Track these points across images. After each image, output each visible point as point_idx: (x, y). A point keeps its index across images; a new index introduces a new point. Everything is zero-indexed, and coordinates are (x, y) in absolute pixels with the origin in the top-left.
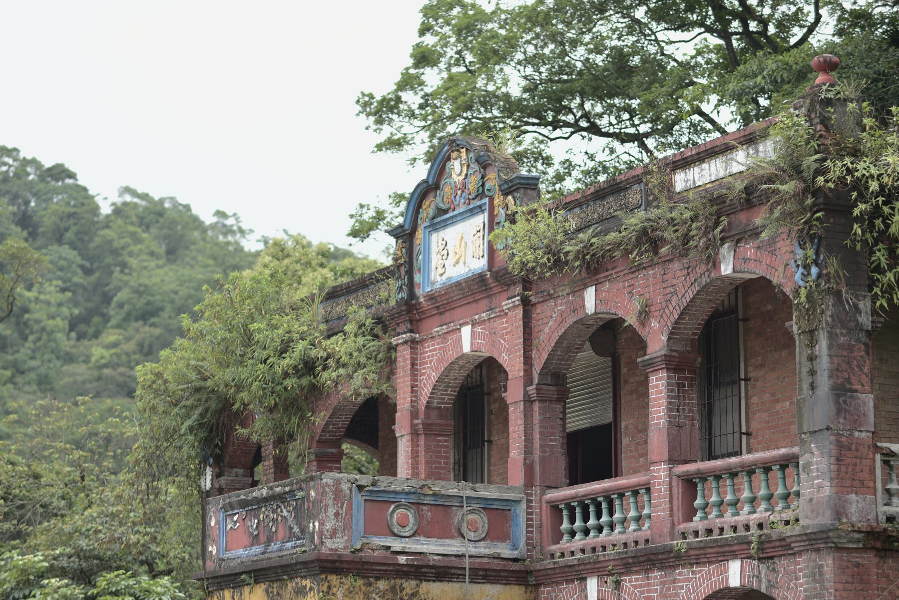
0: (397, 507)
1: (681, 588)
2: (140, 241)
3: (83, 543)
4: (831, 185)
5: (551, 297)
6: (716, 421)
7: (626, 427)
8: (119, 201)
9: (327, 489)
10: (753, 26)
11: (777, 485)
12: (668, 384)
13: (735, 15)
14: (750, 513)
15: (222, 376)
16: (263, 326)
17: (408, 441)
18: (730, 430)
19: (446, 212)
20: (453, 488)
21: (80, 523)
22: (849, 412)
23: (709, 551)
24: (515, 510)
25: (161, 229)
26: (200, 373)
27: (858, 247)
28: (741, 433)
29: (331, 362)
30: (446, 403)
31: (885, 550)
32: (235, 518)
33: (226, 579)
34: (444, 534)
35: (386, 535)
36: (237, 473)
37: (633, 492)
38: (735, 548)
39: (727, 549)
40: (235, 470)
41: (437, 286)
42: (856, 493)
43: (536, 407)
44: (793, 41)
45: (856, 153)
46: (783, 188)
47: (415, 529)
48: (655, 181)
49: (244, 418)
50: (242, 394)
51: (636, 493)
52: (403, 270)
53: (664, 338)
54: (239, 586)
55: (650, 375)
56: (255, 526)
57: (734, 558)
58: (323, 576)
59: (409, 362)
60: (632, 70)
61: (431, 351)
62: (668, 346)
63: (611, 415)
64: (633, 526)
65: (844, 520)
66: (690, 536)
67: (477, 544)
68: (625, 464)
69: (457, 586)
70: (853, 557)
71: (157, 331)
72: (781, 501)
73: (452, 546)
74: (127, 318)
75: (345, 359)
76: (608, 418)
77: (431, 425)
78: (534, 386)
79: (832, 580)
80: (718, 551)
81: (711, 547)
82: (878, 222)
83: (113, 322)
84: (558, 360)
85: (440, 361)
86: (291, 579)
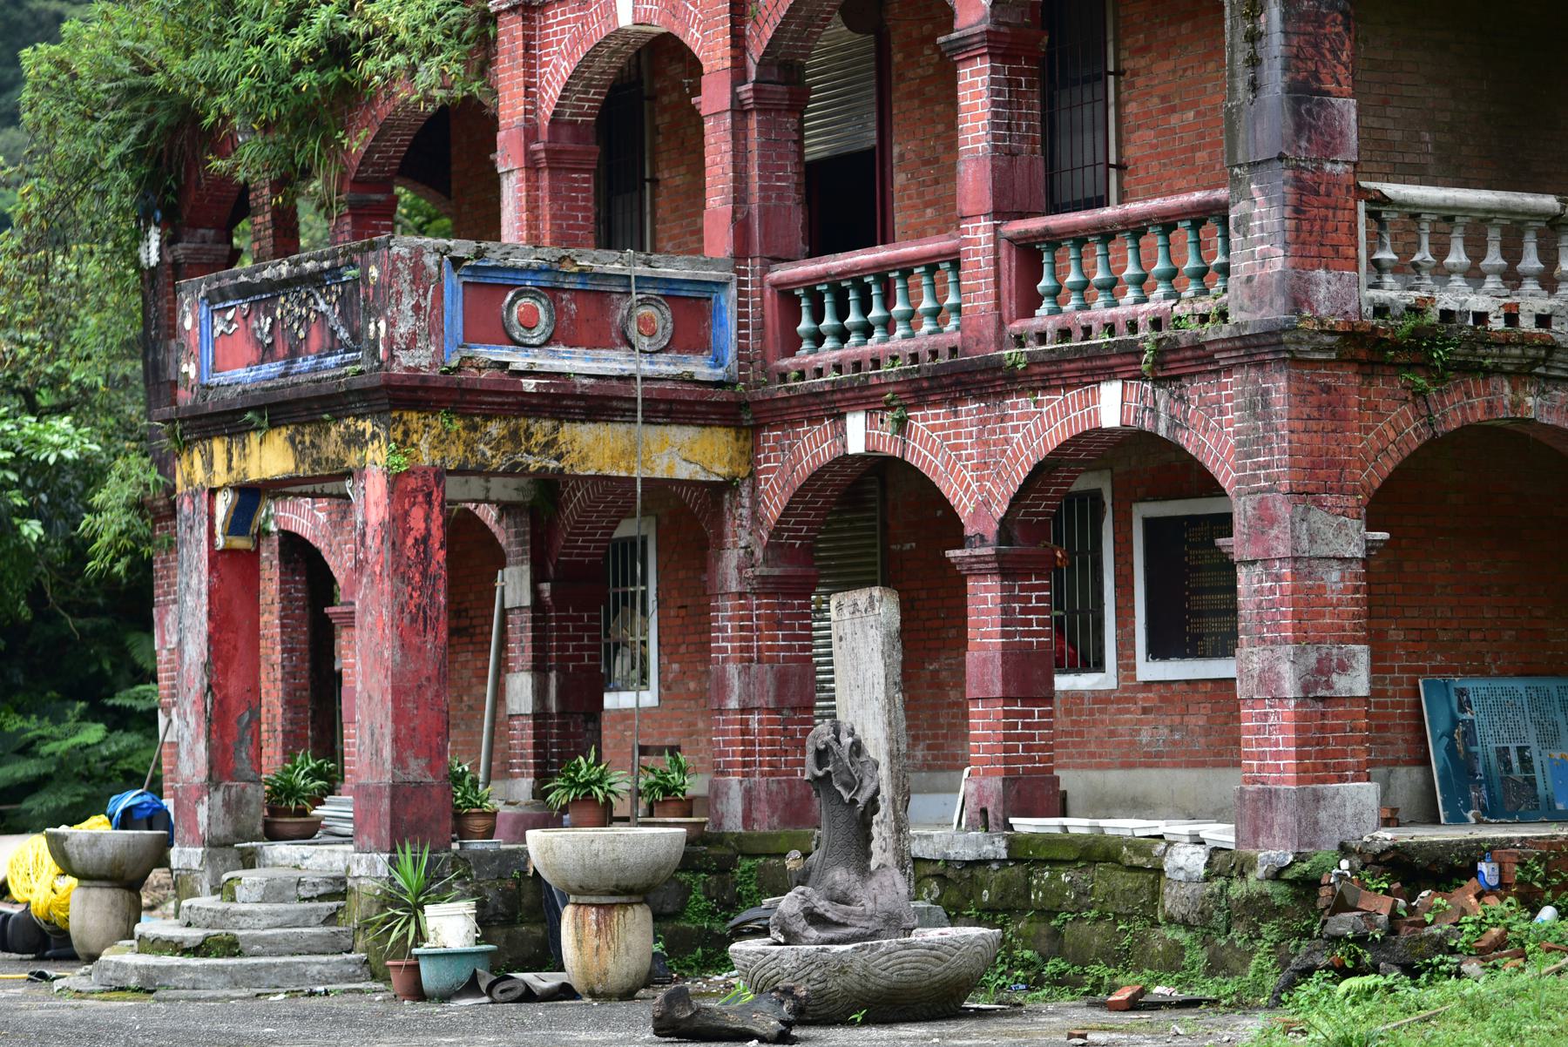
0: (518, 296)
1: (1016, 429)
6: (1063, 145)
7: (902, 156)
9: (400, 265)
11: (1125, 259)
12: (993, 81)
14: (1137, 302)
17: (519, 181)
18: (1088, 160)
22: (1316, 128)
23: (1067, 366)
24: (718, 299)
26: (136, 61)
28: (1109, 166)
29: (379, 43)
30: (585, 115)
31: (1372, 363)
32: (230, 315)
33: (215, 420)
34: (599, 341)
35: (499, 343)
36: (203, 236)
37: (927, 266)
38: (1112, 361)
39: (1099, 363)
40: (201, 231)
42: (1327, 268)
43: (753, 122)
47: (549, 331)
50: (219, 100)
51: (932, 269)
54: (241, 433)
55: (960, 65)
56: (266, 329)
57: (1110, 379)
58: (395, 414)
59: (520, 42)
61: (558, 24)
62: (992, 15)
63: (874, 134)
64: (927, 326)
65: (1307, 314)
66: (1031, 342)
67: (655, 358)
68: (899, 220)
69: (621, 429)
70: (1320, 375)
72: (1192, 282)
73: (613, 362)
75: (404, 36)
76: (871, 138)
77: (561, 152)
78: (750, 86)
79: (1285, 414)
80: (1080, 366)
81: (1070, 361)
84: (791, 39)
85: (575, 41)
86: (338, 419)
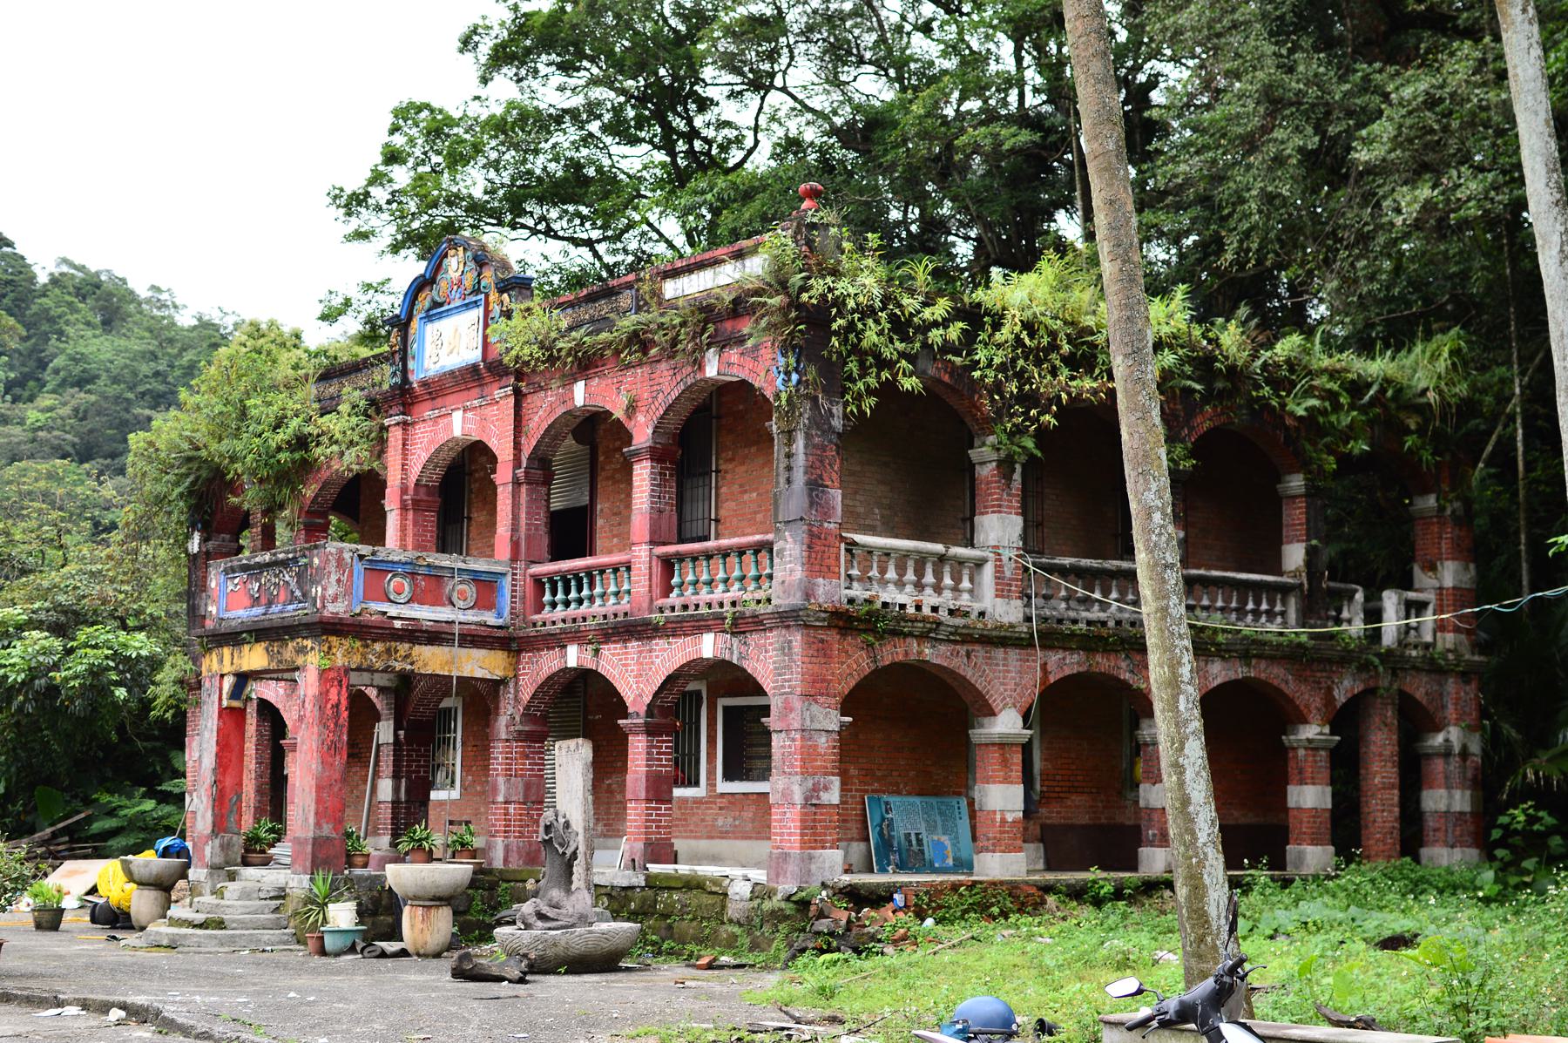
2: (77, 311)
3: (62, 598)
4: (814, 301)
5: (542, 389)
6: (687, 508)
8: (56, 271)
10: (697, 145)
13: (681, 135)
15: (217, 449)
16: (259, 402)
19: (441, 305)
20: (445, 560)
21: (57, 580)
25: (97, 300)
26: (191, 443)
27: (834, 357)
29: (324, 439)
34: (436, 602)
41: (431, 373)
43: (524, 489)
44: (731, 164)
45: (835, 273)
46: (770, 301)
48: (646, 287)
49: (234, 487)
51: (616, 570)
52: (397, 357)
53: (650, 431)
60: (588, 181)
64: (612, 600)
68: (599, 543)
71: (93, 398)
73: (443, 614)
74: (63, 384)
75: (338, 436)
76: (586, 500)
80: (693, 624)
82: (852, 336)
83: (49, 387)
85: (431, 442)
86: (292, 639)
